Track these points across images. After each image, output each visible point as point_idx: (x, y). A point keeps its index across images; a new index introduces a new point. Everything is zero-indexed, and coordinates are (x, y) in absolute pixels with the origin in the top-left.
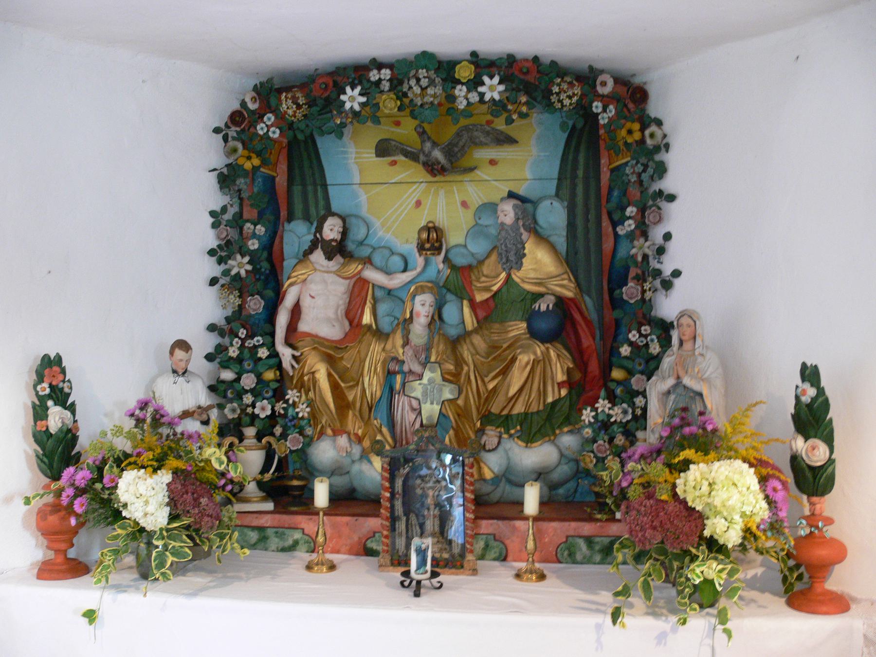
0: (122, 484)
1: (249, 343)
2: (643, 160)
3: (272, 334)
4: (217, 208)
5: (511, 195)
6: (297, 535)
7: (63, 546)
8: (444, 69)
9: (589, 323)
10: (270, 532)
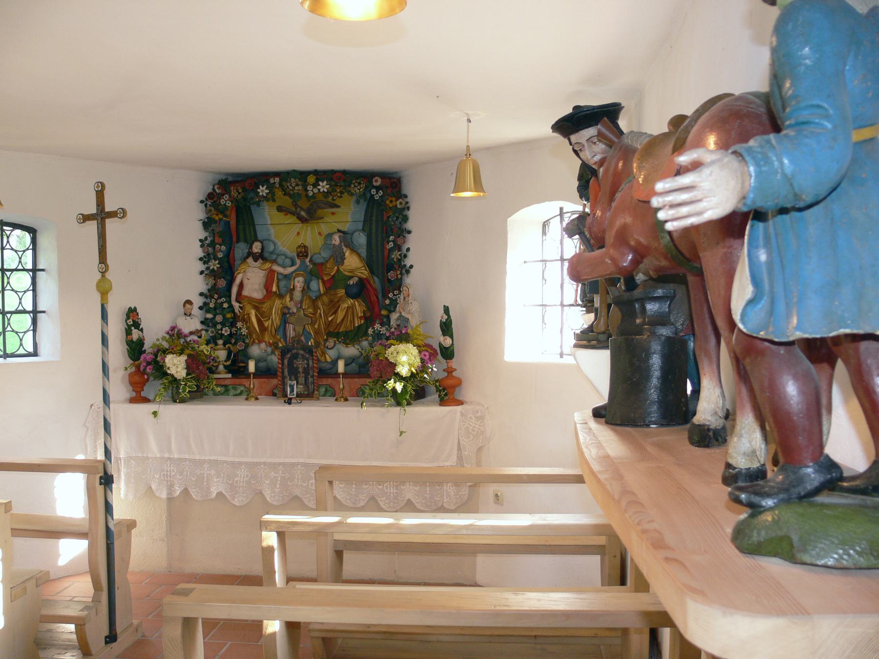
0: (167, 360)
1: (220, 301)
2: (397, 215)
3: (230, 297)
4: (203, 238)
5: (339, 231)
6: (242, 388)
7: (139, 389)
8: (302, 175)
9: (375, 290)
10: (230, 387)
